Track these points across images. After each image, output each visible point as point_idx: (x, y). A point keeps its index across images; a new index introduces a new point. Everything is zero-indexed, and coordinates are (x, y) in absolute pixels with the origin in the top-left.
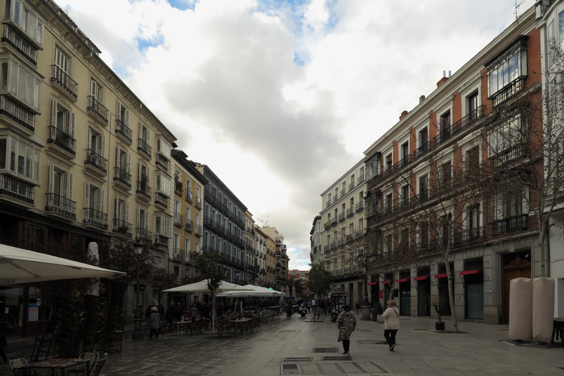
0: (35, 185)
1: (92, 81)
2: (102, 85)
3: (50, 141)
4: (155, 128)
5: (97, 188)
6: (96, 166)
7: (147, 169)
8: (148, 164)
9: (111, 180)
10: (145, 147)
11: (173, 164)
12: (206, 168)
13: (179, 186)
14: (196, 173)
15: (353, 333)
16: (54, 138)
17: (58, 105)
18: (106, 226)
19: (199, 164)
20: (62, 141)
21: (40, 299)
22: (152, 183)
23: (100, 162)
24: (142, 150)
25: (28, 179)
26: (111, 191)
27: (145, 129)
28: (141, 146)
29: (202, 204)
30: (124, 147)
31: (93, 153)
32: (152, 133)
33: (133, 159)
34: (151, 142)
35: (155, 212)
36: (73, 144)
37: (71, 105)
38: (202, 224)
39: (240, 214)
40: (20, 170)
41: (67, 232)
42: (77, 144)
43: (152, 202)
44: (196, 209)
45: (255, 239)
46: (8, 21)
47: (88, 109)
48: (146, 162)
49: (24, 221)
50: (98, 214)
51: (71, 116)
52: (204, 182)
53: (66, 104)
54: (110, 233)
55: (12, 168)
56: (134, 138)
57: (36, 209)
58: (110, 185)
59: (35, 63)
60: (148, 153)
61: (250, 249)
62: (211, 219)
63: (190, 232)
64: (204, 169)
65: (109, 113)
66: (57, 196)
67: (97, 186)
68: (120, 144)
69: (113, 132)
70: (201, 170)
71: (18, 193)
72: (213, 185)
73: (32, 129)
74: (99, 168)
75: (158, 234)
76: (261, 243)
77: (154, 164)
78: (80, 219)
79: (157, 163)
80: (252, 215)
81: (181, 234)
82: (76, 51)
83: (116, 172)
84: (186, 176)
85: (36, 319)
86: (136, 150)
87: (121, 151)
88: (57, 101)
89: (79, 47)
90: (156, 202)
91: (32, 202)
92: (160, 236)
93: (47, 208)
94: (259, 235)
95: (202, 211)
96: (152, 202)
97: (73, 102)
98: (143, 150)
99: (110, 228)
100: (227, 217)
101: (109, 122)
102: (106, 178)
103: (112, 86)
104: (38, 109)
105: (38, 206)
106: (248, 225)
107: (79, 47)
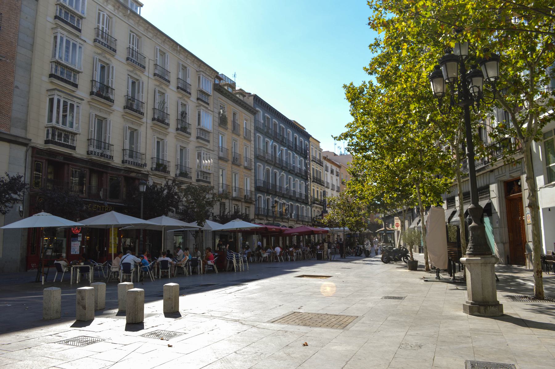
0: (76, 134)
1: (132, 34)
2: (165, 52)
3: (92, 93)
4: (195, 65)
5: (136, 130)
6: (134, 110)
7: (187, 106)
8: (189, 101)
9: (150, 121)
10: (186, 86)
11: (216, 99)
12: (257, 99)
13: (223, 121)
14: (245, 105)
15: (350, 104)
16: (179, 127)
17: (100, 60)
18: (145, 165)
19: (250, 94)
20: (102, 93)
21: (81, 234)
22: (191, 119)
23: (138, 105)
24: (158, 75)
25: (70, 129)
26: (150, 131)
27: (184, 68)
28: (180, 86)
29: (252, 135)
30: (162, 88)
31: (133, 99)
32: (192, 69)
33: (172, 97)
34: (191, 80)
35: (196, 147)
36: (112, 93)
37: (111, 58)
38: (253, 157)
39: (301, 142)
40: (64, 123)
41: (107, 173)
42: (116, 92)
43: (193, 138)
44: (245, 141)
45: (324, 168)
46: (58, 3)
47: (128, 59)
48: (186, 99)
49: (68, 164)
50: (105, 146)
51: (111, 69)
52: (254, 112)
53: (107, 58)
54: (148, 172)
55: (58, 122)
56: (173, 78)
57: (79, 154)
58: (149, 126)
59: (80, 31)
60: (188, 90)
61: (319, 181)
62: (286, 162)
63: (239, 166)
64: (254, 98)
65: (147, 60)
66: (101, 142)
67: (136, 128)
68: (158, 86)
69: (151, 76)
70: (250, 102)
71: (62, 142)
72: (281, 125)
73: (76, 86)
74: (136, 111)
75: (50, 124)
76: (332, 172)
77: (195, 100)
78: (117, 161)
79: (198, 99)
80: (319, 142)
81: (228, 166)
82: (116, 11)
83: (154, 113)
84: (230, 108)
85: (78, 253)
86: (175, 89)
87: (159, 92)
88: (99, 57)
89: (119, 7)
90: (198, 138)
91: (74, 148)
92: (201, 171)
93: (123, 162)
94: (329, 165)
95: (253, 142)
96: (193, 138)
97: (113, 56)
98: (183, 89)
99: (148, 168)
100: (285, 146)
101: (147, 68)
102: (144, 120)
103: (150, 35)
104: (80, 69)
105: (81, 151)
106: (313, 153)
107: (119, 7)
